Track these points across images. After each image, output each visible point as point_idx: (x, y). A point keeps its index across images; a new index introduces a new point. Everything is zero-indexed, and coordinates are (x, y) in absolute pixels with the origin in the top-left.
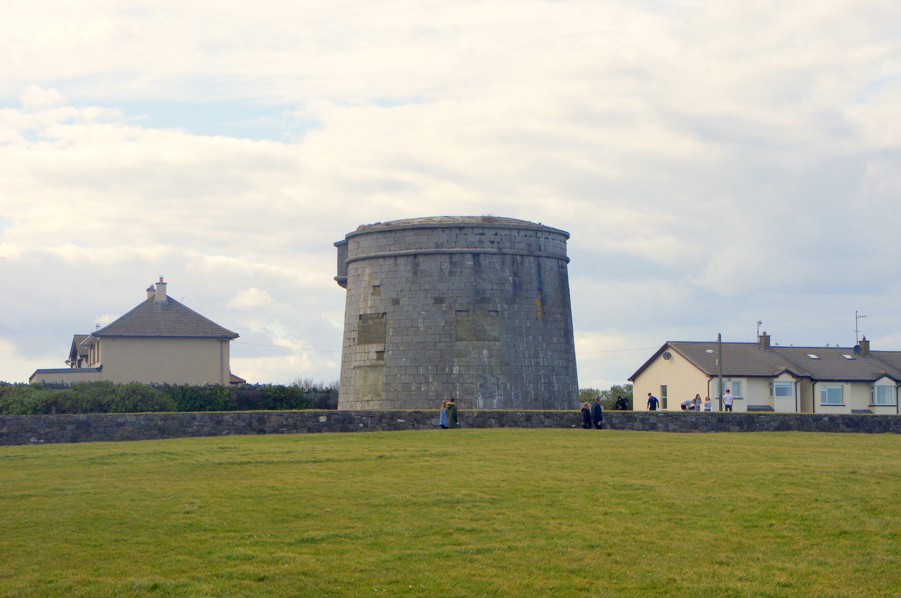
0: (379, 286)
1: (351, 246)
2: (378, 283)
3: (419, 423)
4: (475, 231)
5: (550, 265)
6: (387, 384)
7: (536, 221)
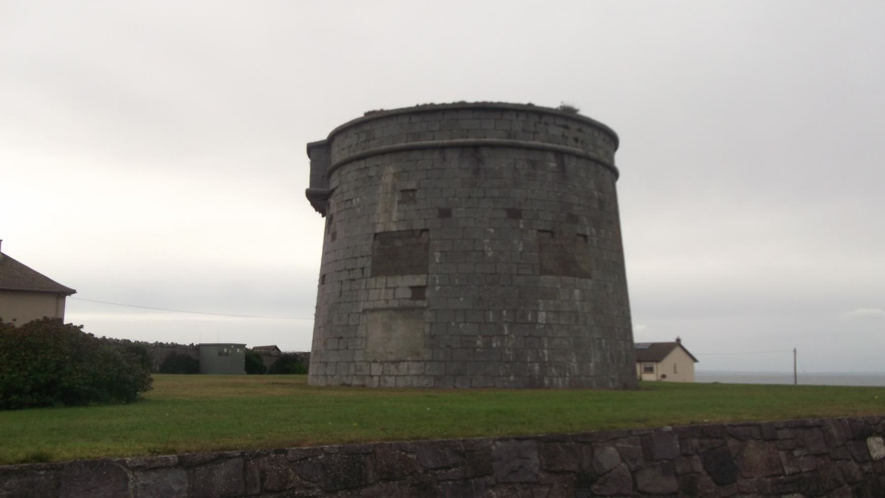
2: (412, 185)
6: (432, 337)
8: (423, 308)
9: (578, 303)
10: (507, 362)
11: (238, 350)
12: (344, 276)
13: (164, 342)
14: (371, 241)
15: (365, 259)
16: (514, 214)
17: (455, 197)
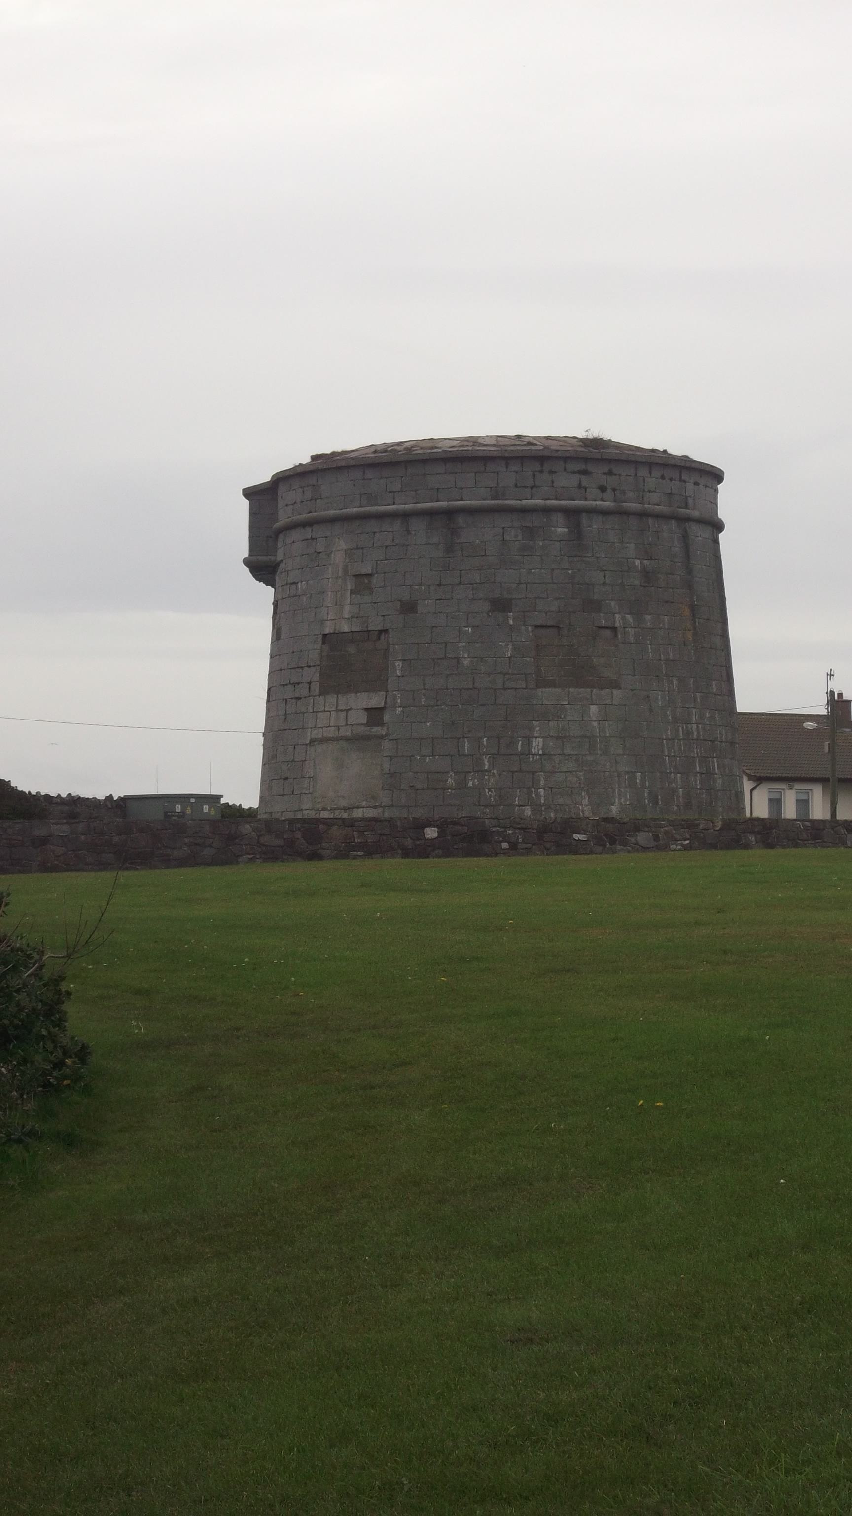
0: (370, 575)
1: (287, 495)
3: (613, 843)
4: (572, 466)
5: (699, 533)
6: (392, 775)
7: (677, 450)
8: (382, 737)
9: (595, 724)
10: (486, 806)
11: (206, 809)
12: (289, 692)
13: (53, 794)
14: (319, 646)
15: (313, 669)
16: (501, 605)
17: (421, 585)
